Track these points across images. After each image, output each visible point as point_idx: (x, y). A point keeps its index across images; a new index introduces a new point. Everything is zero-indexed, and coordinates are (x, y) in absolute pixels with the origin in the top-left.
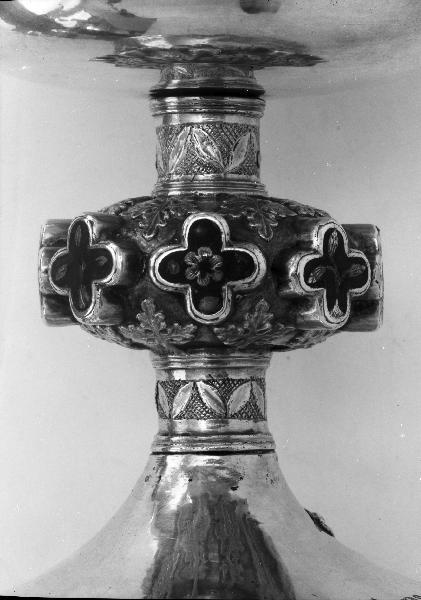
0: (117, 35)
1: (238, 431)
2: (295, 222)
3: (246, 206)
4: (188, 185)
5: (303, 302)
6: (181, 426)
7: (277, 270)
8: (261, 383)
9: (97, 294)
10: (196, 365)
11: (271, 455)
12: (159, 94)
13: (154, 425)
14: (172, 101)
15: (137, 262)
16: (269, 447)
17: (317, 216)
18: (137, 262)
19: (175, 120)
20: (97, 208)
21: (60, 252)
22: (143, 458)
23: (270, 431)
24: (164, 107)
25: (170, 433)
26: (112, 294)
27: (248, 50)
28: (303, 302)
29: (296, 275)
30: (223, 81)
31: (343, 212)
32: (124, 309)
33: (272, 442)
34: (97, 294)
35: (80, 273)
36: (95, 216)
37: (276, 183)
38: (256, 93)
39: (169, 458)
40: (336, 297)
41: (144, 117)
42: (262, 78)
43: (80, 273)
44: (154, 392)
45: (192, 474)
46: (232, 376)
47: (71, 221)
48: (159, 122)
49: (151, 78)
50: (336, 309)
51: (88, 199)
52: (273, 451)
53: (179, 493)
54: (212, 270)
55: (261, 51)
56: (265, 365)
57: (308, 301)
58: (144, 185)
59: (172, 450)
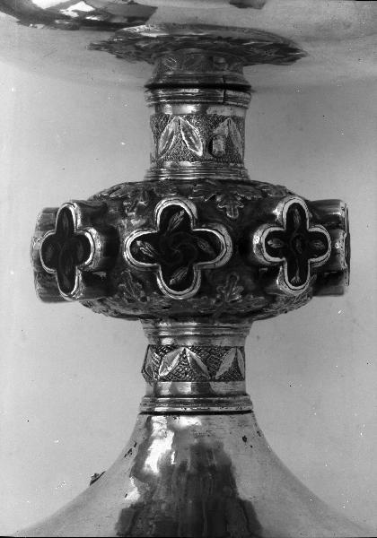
0: (112, 32)
1: (216, 388)
2: (259, 201)
3: (229, 192)
4: (175, 170)
5: (273, 271)
6: (166, 387)
7: (242, 244)
8: (242, 349)
9: (78, 277)
10: (187, 333)
11: (248, 415)
12: (152, 87)
13: (141, 388)
14: (161, 92)
15: (113, 246)
16: (245, 408)
17: (283, 193)
18: (113, 246)
19: (168, 110)
20: (85, 196)
21: (50, 233)
22: (133, 418)
23: (247, 392)
24: (157, 98)
25: (155, 395)
26: (89, 278)
27: (228, 39)
28: (273, 271)
29: (259, 246)
30: (211, 68)
31: (307, 187)
32: (107, 287)
33: (249, 403)
34: (78, 277)
35: (70, 257)
36: (81, 204)
37: (258, 168)
38: (245, 88)
39: (155, 418)
40: (298, 270)
41: (140, 103)
42: (252, 74)
43: (70, 257)
44: (144, 358)
45: (179, 435)
46: (217, 343)
47: (57, 209)
48: (153, 112)
49: (147, 72)
50: (297, 278)
51: (79, 185)
52: (250, 411)
53: (161, 449)
54: (175, 247)
55: (97, 49)
56: (245, 334)
57: (41, 230)
58: (137, 172)
59: (158, 409)
